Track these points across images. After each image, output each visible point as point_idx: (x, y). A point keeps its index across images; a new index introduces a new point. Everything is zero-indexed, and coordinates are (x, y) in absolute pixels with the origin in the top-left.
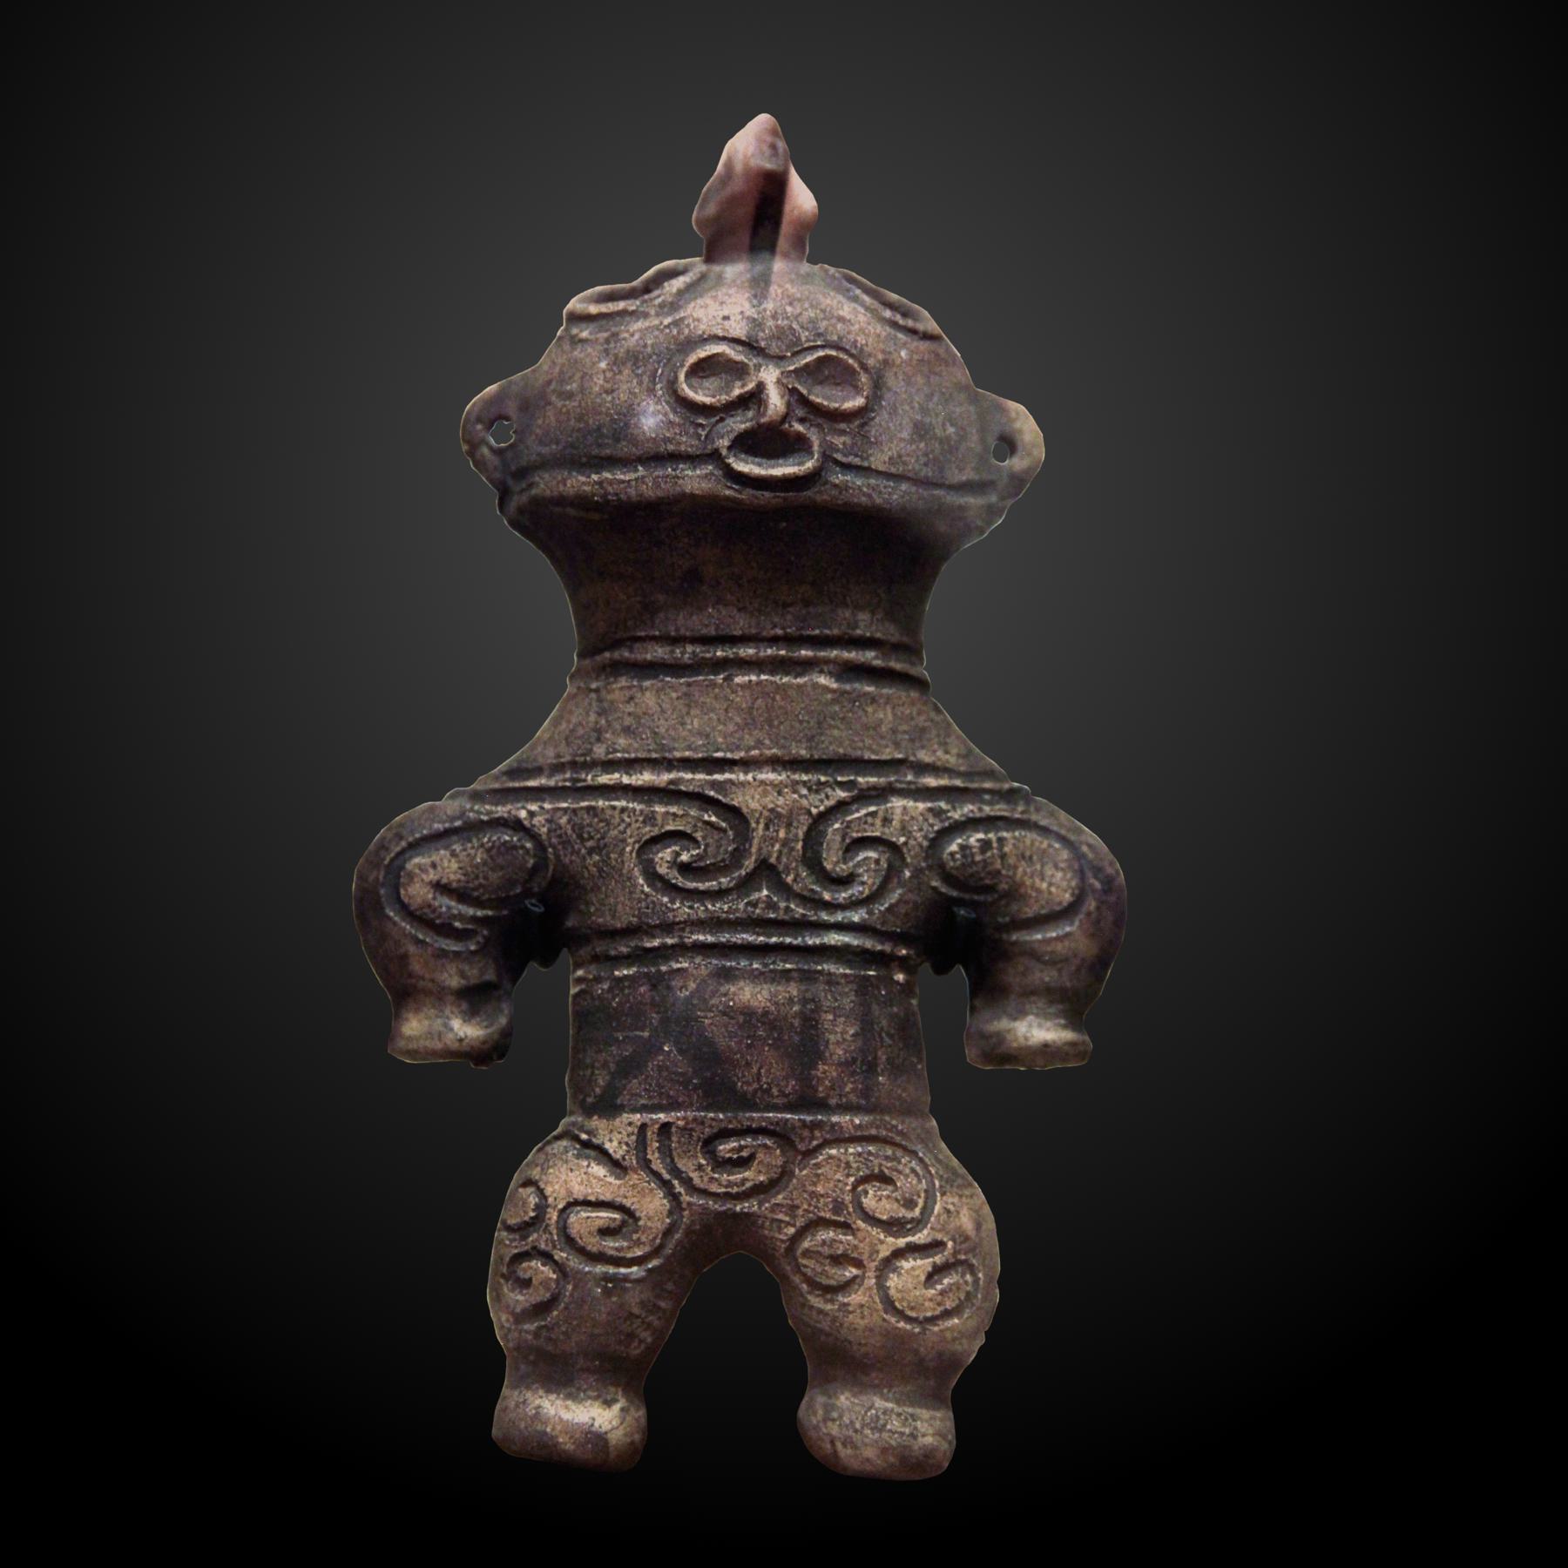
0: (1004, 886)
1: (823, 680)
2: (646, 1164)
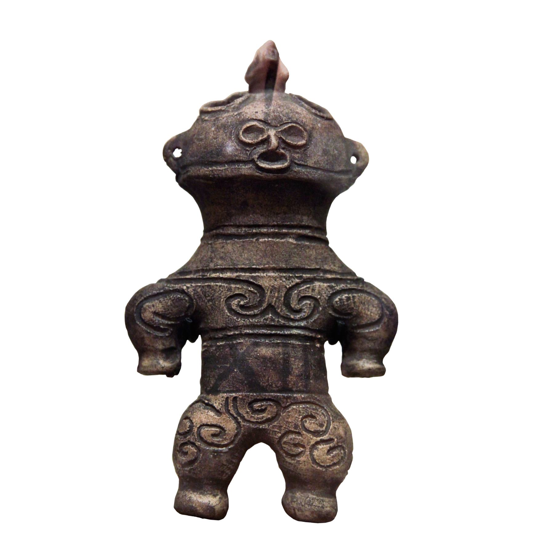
0: (355, 313)
1: (291, 240)
2: (228, 411)
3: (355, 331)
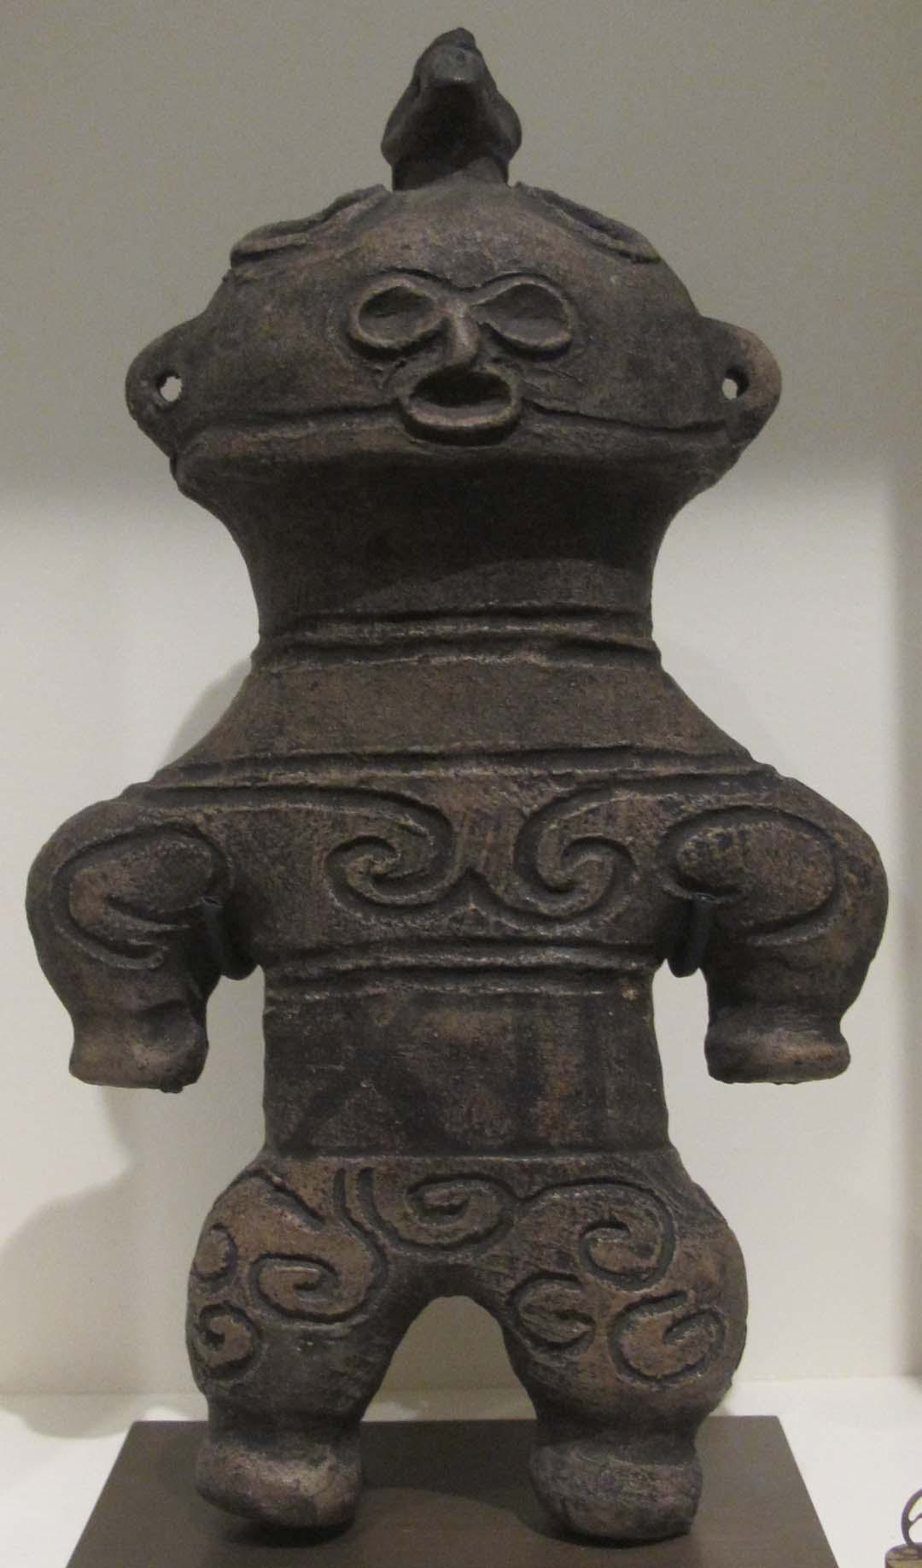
0: (747, 886)
1: (532, 658)
2: (346, 1212)
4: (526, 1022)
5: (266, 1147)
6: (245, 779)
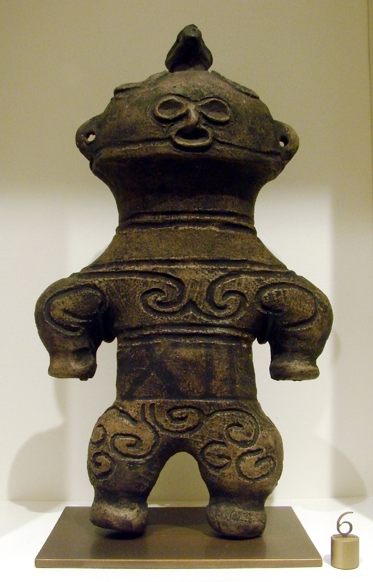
1: (213, 228)
2: (145, 420)
3: (286, 330)
4: (209, 353)
5: (117, 399)
6: (113, 269)
